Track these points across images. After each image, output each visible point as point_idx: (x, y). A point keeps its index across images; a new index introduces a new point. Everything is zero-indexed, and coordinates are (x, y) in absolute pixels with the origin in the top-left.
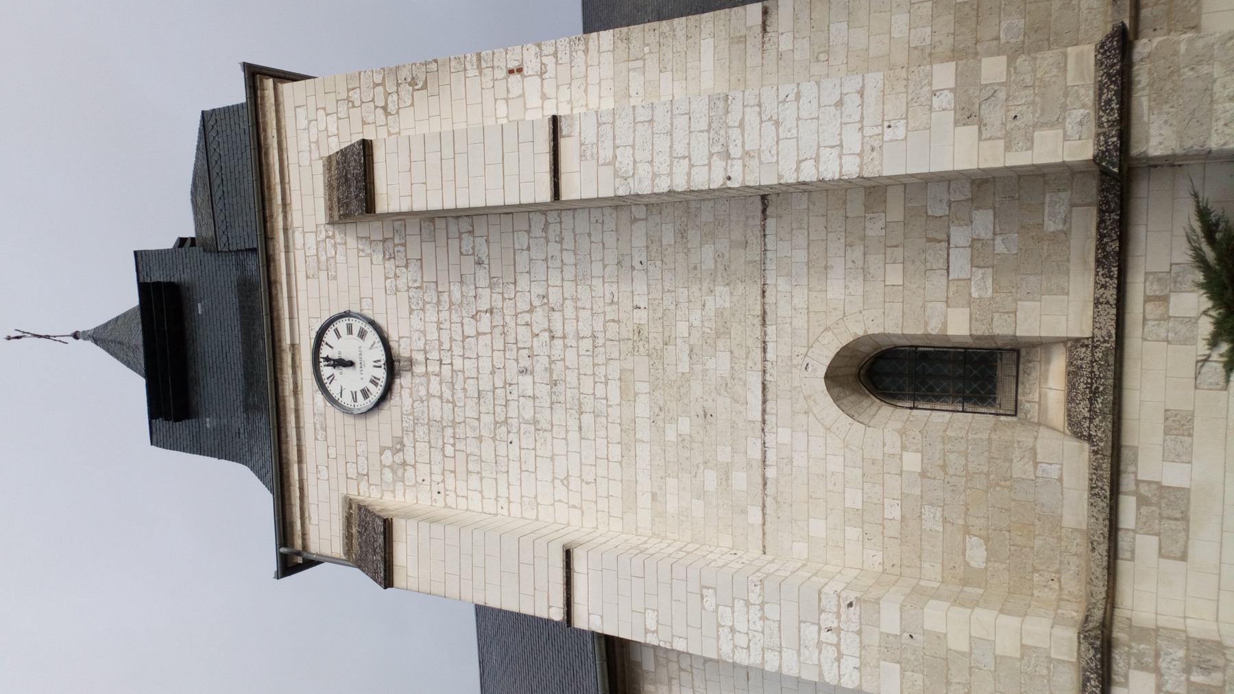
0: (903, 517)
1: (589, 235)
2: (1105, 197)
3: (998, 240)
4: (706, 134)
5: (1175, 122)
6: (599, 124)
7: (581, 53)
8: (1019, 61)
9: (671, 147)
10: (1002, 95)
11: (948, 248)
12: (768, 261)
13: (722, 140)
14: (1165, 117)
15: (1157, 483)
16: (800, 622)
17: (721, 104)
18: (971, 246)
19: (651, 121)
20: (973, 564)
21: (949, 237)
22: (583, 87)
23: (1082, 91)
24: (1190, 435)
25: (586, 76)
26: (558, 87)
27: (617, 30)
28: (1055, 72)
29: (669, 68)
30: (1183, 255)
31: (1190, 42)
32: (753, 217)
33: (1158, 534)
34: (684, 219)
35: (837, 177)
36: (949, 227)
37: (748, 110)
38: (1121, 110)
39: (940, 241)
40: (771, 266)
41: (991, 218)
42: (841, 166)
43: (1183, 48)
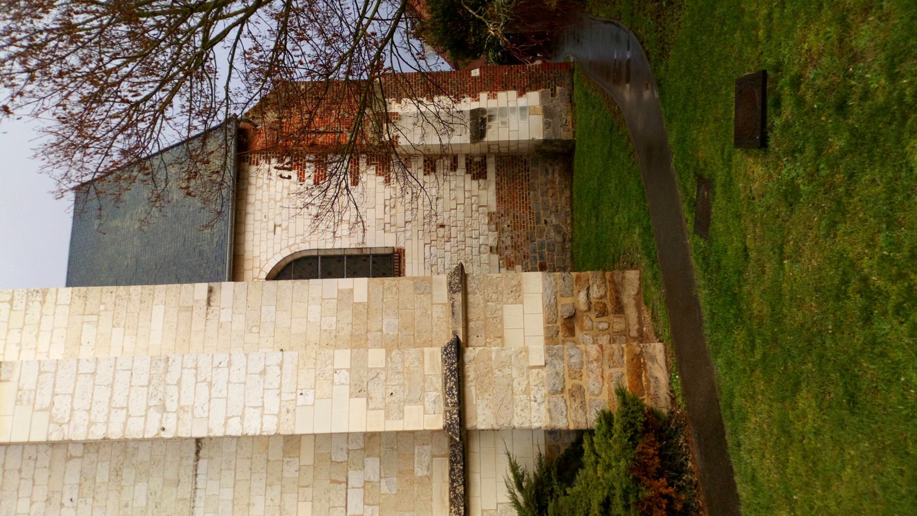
1: (20, 471)
2: (454, 451)
3: (383, 481)
4: (145, 388)
5: (492, 406)
6: (40, 373)
7: (37, 304)
8: (393, 353)
9: (111, 398)
10: (382, 377)
11: (347, 489)
12: (197, 499)
13: (160, 395)
14: (486, 402)
17: (162, 365)
18: (364, 487)
19: (94, 374)
21: (347, 479)
22: (35, 333)
23: (434, 379)
25: (39, 324)
26: (8, 330)
27: (76, 289)
28: (416, 364)
29: (122, 324)
30: (505, 498)
31: (498, 352)
32: (187, 458)
34: (121, 458)
35: (258, 433)
36: (347, 471)
37: (185, 371)
38: (459, 395)
39: (340, 483)
40: (199, 503)
41: (378, 465)
42: (262, 424)
43: (494, 356)
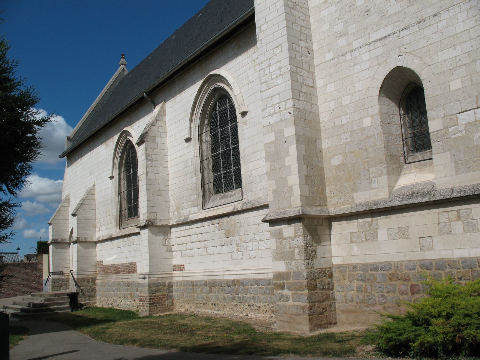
0: (343, 125)
15: (378, 228)
16: (279, 94)
20: (332, 160)
24: (399, 238)
33: (358, 231)
39: (477, 103)
